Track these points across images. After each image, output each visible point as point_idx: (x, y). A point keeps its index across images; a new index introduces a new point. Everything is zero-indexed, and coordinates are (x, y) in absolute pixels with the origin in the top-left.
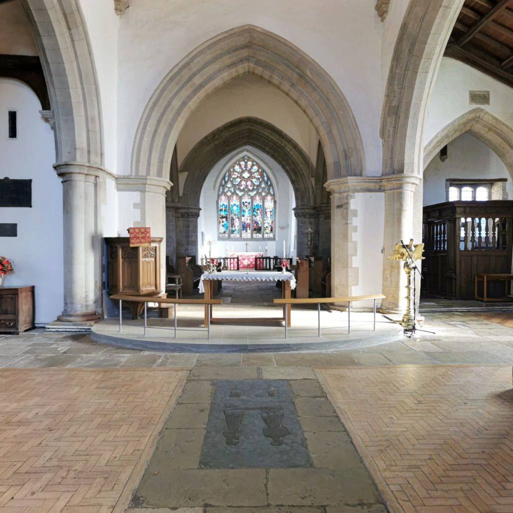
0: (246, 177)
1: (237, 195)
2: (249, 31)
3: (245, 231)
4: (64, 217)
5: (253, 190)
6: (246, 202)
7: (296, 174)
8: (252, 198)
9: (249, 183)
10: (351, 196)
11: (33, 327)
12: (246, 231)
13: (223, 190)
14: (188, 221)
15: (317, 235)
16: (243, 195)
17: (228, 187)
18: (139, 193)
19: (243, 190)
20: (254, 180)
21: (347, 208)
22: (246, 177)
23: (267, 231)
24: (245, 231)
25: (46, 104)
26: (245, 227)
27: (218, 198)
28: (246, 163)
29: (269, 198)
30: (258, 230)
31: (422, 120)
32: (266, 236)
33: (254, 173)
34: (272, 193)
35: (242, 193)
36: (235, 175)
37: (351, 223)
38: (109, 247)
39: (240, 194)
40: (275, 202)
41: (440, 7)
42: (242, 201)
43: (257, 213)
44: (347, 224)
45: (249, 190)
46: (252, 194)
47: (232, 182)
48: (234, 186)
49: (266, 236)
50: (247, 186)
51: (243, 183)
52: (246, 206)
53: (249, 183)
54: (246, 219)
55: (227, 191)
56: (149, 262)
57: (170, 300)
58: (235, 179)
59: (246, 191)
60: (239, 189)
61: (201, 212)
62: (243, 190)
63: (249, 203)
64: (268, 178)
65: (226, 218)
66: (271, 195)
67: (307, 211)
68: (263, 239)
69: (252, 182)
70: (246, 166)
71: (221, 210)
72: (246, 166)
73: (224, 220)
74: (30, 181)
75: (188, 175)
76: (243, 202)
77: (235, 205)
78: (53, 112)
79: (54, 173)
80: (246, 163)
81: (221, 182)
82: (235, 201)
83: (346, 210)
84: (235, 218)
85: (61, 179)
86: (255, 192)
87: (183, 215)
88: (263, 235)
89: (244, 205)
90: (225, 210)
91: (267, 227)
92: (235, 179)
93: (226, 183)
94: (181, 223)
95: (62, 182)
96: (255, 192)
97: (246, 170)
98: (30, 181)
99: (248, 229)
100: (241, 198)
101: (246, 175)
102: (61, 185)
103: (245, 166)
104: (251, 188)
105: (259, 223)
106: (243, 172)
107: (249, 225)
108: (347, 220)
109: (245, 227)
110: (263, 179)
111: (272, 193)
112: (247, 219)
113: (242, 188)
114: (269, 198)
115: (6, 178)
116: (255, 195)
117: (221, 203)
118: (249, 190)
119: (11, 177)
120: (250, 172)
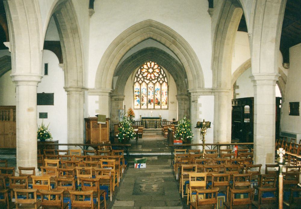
0: (151, 72)
1: (145, 82)
2: (150, 21)
3: (150, 104)
4: (68, 111)
5: (155, 79)
6: (151, 87)
7: (177, 76)
8: (154, 84)
9: (152, 75)
10: (198, 97)
11: (114, 152)
12: (151, 104)
13: (137, 79)
14: (118, 103)
15: (189, 111)
16: (149, 83)
17: (139, 78)
18: (98, 96)
19: (149, 80)
20: (155, 74)
21: (196, 103)
22: (151, 72)
23: (163, 104)
24: (150, 104)
25: (61, 61)
26: (150, 101)
27: (134, 84)
28: (151, 63)
29: (164, 84)
30: (158, 103)
31: (200, 91)
32: (163, 107)
33: (155, 69)
34: (166, 81)
35: (149, 81)
36: (144, 71)
37: (199, 110)
38: (86, 123)
39: (147, 82)
40: (168, 87)
41: (230, 21)
42: (148, 86)
43: (157, 93)
44: (197, 110)
45: (153, 80)
46: (154, 82)
47: (142, 75)
48: (143, 77)
49: (163, 107)
50: (151, 77)
51: (149, 75)
52: (151, 89)
53: (152, 75)
54: (151, 97)
55: (139, 80)
56: (223, 198)
57: (97, 146)
58: (144, 73)
59: (151, 80)
60: (146, 79)
61: (125, 98)
62: (149, 80)
63: (152, 87)
64: (164, 73)
65: (139, 96)
66: (166, 83)
67: (183, 97)
68: (161, 109)
69: (154, 74)
70: (151, 65)
71: (136, 92)
72: (151, 65)
73: (137, 97)
74: (53, 94)
75: (119, 78)
76: (149, 87)
77: (144, 88)
78: (64, 65)
79: (64, 90)
80: (151, 63)
81: (136, 75)
82: (144, 86)
83: (196, 104)
84: (144, 96)
85: (66, 93)
86: (156, 81)
87: (115, 100)
88: (161, 107)
89: (149, 88)
90: (138, 92)
91: (163, 102)
92: (144, 73)
93: (139, 75)
94: (114, 104)
95: (67, 94)
96: (156, 81)
97: (151, 68)
98: (53, 94)
99: (152, 103)
100: (147, 84)
101: (151, 70)
102: (67, 95)
103: (150, 68)
104: (153, 78)
105: (159, 99)
106: (149, 68)
107: (152, 101)
108: (197, 108)
109: (150, 101)
110: (161, 73)
111: (166, 81)
112: (151, 97)
113: (148, 78)
114: (164, 84)
115: (43, 93)
116: (156, 82)
117: (135, 87)
118: (153, 80)
119: (45, 92)
120: (153, 68)
